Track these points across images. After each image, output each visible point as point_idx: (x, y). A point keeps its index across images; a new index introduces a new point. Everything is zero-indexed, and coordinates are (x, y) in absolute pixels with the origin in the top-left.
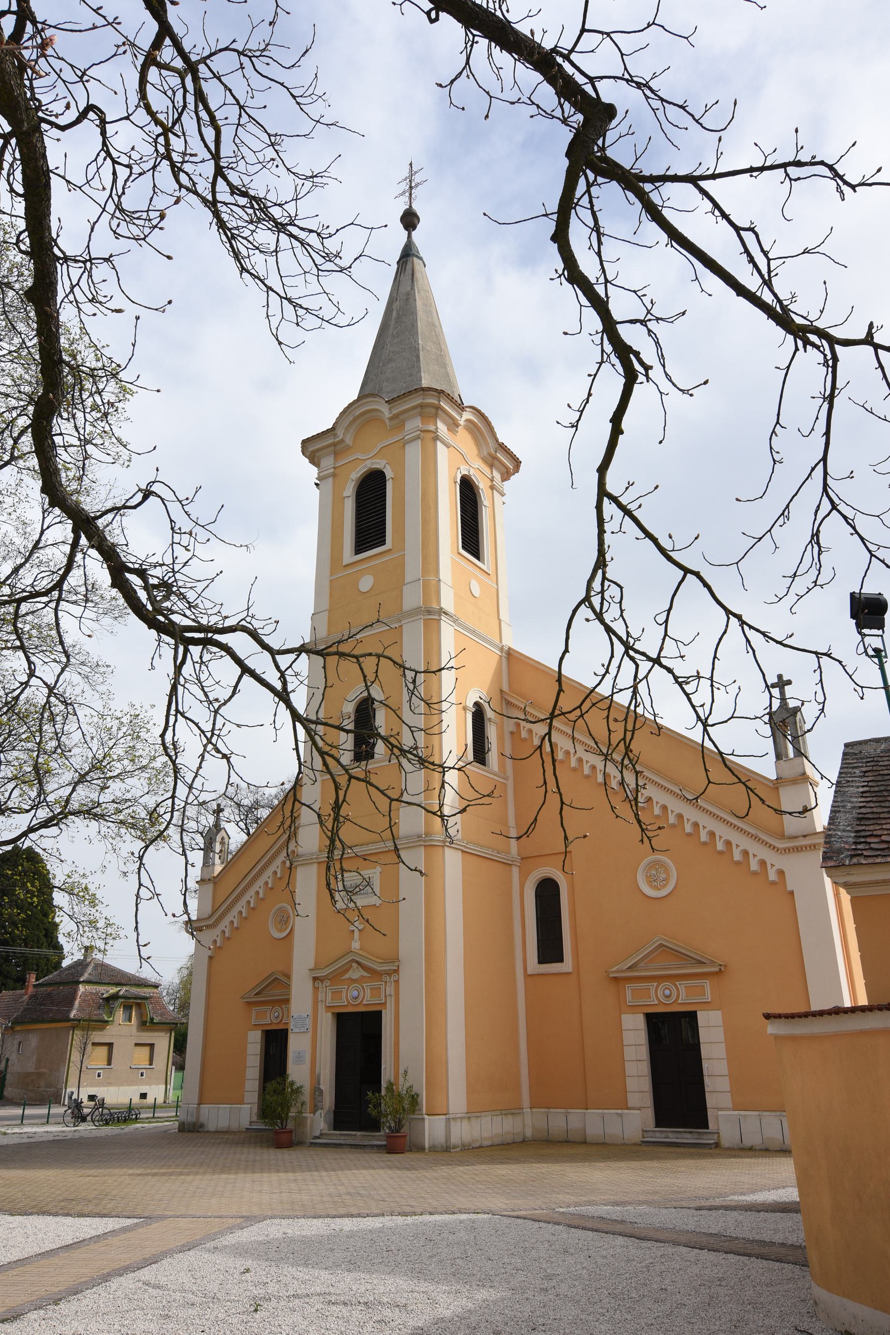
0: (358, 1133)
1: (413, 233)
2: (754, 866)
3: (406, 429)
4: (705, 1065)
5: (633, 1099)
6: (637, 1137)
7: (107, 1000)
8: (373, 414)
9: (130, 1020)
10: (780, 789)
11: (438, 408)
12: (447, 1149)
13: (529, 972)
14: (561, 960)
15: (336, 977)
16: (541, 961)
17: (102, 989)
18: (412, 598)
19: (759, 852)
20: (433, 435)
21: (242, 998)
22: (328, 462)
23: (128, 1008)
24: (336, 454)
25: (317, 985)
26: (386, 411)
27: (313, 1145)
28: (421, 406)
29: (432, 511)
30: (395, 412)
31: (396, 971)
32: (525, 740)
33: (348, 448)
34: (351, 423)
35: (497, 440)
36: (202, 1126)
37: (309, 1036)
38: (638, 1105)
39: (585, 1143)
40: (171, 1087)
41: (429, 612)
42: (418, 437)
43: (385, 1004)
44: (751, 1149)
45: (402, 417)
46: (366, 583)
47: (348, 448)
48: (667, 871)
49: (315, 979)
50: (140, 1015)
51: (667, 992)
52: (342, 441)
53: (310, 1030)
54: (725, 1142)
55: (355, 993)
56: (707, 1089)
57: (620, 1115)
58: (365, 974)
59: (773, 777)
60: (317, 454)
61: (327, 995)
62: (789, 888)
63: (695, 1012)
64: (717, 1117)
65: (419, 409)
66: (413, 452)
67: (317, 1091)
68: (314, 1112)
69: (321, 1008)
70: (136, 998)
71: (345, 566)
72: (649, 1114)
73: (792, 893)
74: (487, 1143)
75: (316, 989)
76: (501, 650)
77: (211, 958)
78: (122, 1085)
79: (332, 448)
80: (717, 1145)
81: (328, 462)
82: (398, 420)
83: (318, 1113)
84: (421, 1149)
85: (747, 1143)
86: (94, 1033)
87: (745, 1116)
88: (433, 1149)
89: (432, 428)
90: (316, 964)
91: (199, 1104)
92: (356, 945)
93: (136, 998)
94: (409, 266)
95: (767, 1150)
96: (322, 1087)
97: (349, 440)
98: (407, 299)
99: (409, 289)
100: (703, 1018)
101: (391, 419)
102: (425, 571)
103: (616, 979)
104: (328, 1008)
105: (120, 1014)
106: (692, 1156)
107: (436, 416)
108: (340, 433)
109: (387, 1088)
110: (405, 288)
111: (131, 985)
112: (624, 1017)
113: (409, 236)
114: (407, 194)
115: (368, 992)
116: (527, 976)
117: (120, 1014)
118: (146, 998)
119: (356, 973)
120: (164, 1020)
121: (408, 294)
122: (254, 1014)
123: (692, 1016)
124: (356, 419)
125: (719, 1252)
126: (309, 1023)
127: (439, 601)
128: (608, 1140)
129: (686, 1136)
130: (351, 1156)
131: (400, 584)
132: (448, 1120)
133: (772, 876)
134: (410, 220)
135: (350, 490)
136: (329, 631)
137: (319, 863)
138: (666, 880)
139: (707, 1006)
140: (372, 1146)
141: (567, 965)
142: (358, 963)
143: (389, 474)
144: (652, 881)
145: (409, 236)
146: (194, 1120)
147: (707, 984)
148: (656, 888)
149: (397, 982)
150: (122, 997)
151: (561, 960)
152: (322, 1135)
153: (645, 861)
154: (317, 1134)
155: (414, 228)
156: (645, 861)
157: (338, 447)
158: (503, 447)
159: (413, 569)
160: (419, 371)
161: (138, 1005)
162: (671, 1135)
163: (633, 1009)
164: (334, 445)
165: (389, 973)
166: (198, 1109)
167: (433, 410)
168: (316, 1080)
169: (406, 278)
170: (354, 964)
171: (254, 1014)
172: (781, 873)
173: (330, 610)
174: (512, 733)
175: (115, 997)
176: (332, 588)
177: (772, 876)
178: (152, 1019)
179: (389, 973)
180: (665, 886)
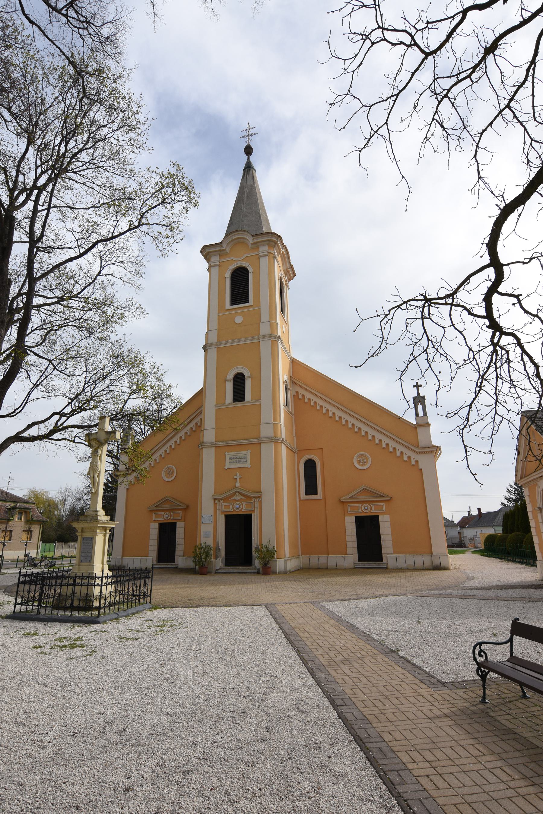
0: (240, 567)
1: (250, 157)
2: (405, 458)
3: (260, 250)
4: (382, 536)
5: (349, 551)
6: (352, 566)
7: (10, 509)
8: (242, 240)
9: (21, 519)
10: (214, 440)
11: (276, 243)
12: (285, 573)
13: (302, 498)
14: (316, 493)
15: (226, 499)
16: (307, 494)
17: (7, 504)
18: (264, 330)
19: (407, 453)
20: (273, 255)
21: (148, 508)
22: (215, 259)
23: (20, 514)
24: (220, 256)
25: (216, 502)
26: (250, 240)
27: (216, 573)
28: (269, 241)
29: (273, 290)
30: (256, 241)
31: (260, 497)
32: (300, 399)
33: (227, 254)
34: (230, 242)
35: (290, 263)
36: (124, 567)
37: (212, 525)
38: (351, 553)
39: (327, 568)
40: (39, 551)
41: (274, 337)
42: (267, 255)
43: (254, 511)
44: (401, 569)
45: (258, 244)
46: (239, 320)
47: (227, 254)
48: (367, 459)
49: (215, 499)
50: (26, 517)
51: (366, 508)
52: (225, 250)
53: (213, 522)
54: (390, 566)
55: (238, 506)
56: (382, 546)
57: (344, 557)
58: (243, 498)
59: (415, 423)
60: (210, 254)
61: (222, 507)
62: (420, 468)
63: (378, 516)
64: (387, 557)
65: (268, 242)
66: (264, 262)
67: (217, 549)
68: (216, 559)
69: (219, 512)
70: (25, 509)
71: (227, 310)
72: (155, 558)
73: (421, 470)
74: (293, 570)
75: (215, 504)
76: (291, 358)
77: (128, 489)
78: (16, 550)
79: (219, 252)
80: (387, 568)
81: (215, 259)
82: (256, 245)
83: (218, 559)
84: (275, 573)
85: (399, 566)
86: (34, 526)
87: (399, 556)
88: (280, 573)
89: (273, 252)
90: (215, 493)
91: (122, 557)
92: (238, 485)
93: (25, 509)
94: (251, 173)
95: (408, 569)
96: (220, 547)
97: (228, 250)
98: (252, 188)
99: (252, 183)
100: (381, 518)
101: (252, 244)
102: (271, 317)
103: (342, 502)
104: (222, 512)
105: (17, 516)
106: (370, 573)
107: (274, 247)
108: (224, 246)
109: (256, 548)
110: (250, 183)
111: (21, 502)
112: (346, 518)
113: (248, 158)
114: (247, 138)
115: (245, 506)
116: (300, 500)
117: (17, 516)
118: (30, 509)
119: (238, 497)
120: (38, 520)
121: (252, 186)
122: (154, 516)
123: (377, 517)
124: (233, 240)
125: (160, 608)
126: (212, 519)
127: (277, 333)
128: (338, 567)
129: (373, 565)
130: (237, 577)
131: (258, 323)
132: (286, 561)
133: (413, 462)
134: (248, 150)
135: (228, 274)
136: (218, 339)
137: (215, 447)
138: (367, 462)
139: (383, 513)
140: (251, 573)
141: (320, 496)
142: (239, 493)
143: (250, 270)
144: (359, 462)
145: (248, 158)
146: (120, 564)
147: (384, 505)
148: (362, 466)
149: (260, 502)
150: (18, 508)
151: (316, 493)
152: (220, 569)
153: (360, 453)
154: (218, 568)
155: (251, 154)
156: (360, 453)
157: (222, 252)
158: (292, 267)
159: (265, 317)
160: (261, 224)
161: (25, 512)
162: (366, 564)
163: (350, 514)
164: (220, 251)
165: (256, 498)
166: (122, 559)
167: (274, 244)
168: (217, 544)
169: (249, 178)
170: (237, 493)
171: (154, 516)
172: (417, 462)
173: (218, 330)
174: (294, 396)
175: (14, 508)
176: (218, 319)
177: (413, 462)
178: (32, 519)
179: (256, 498)
180: (365, 465)
